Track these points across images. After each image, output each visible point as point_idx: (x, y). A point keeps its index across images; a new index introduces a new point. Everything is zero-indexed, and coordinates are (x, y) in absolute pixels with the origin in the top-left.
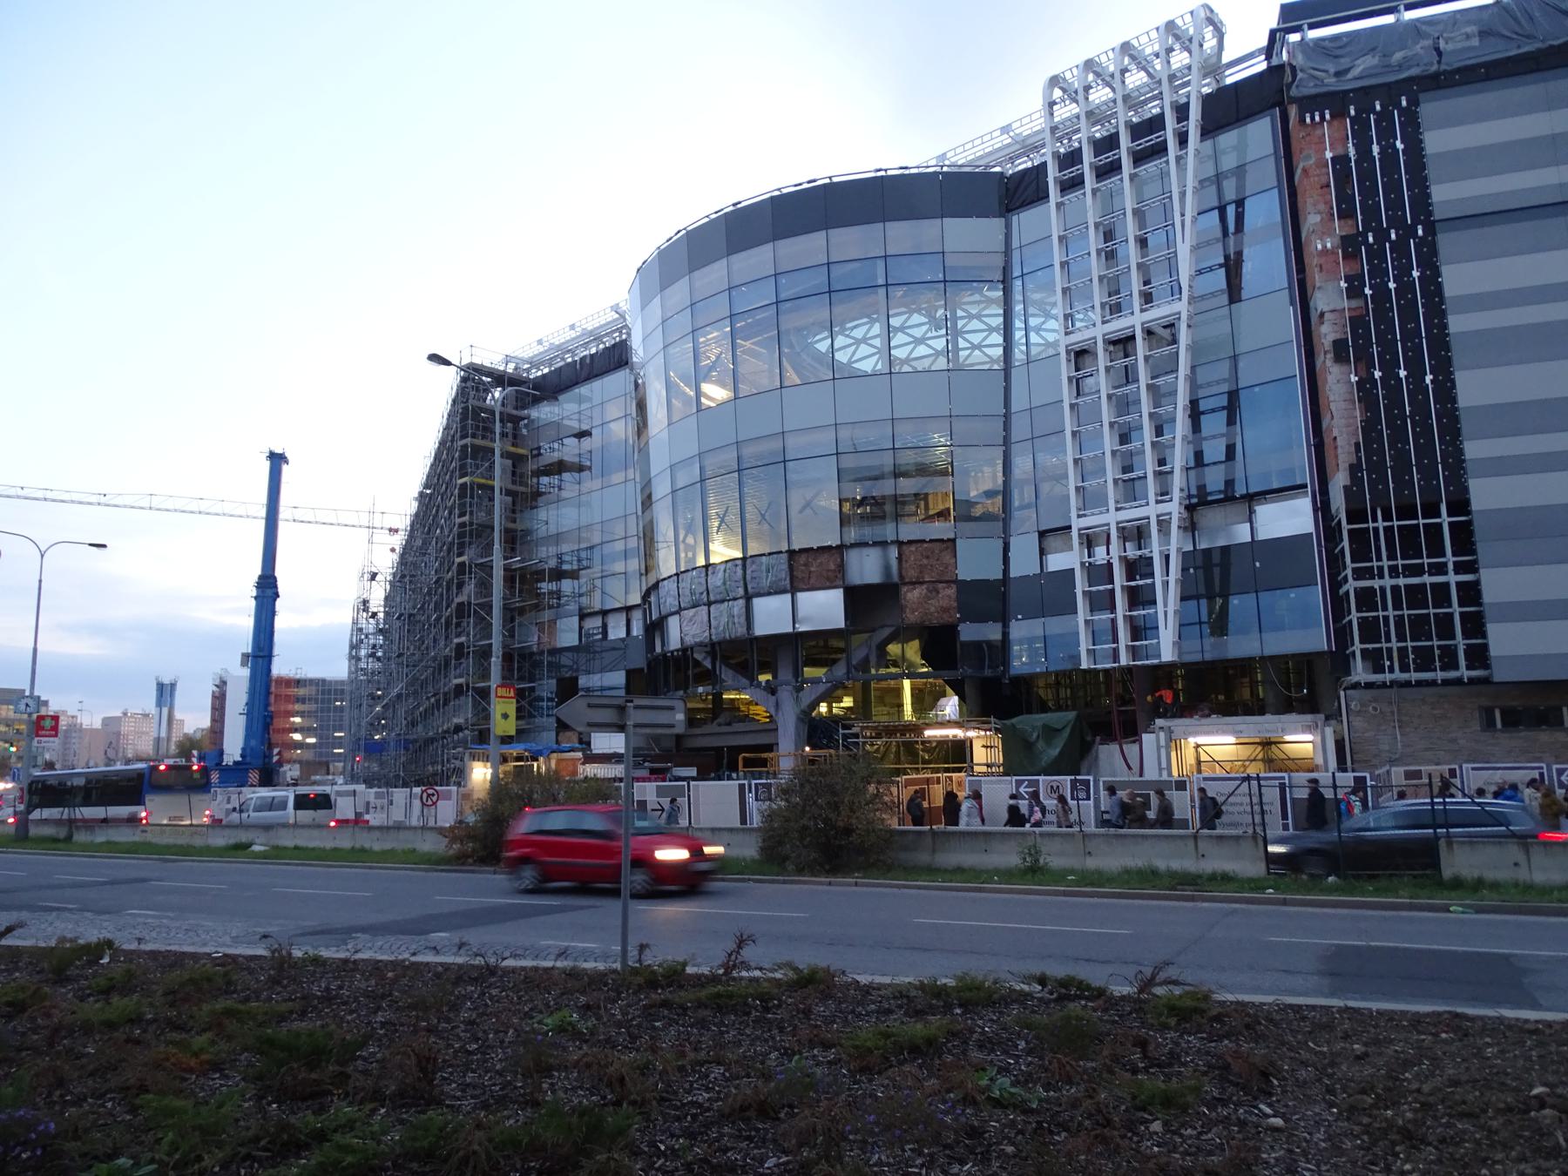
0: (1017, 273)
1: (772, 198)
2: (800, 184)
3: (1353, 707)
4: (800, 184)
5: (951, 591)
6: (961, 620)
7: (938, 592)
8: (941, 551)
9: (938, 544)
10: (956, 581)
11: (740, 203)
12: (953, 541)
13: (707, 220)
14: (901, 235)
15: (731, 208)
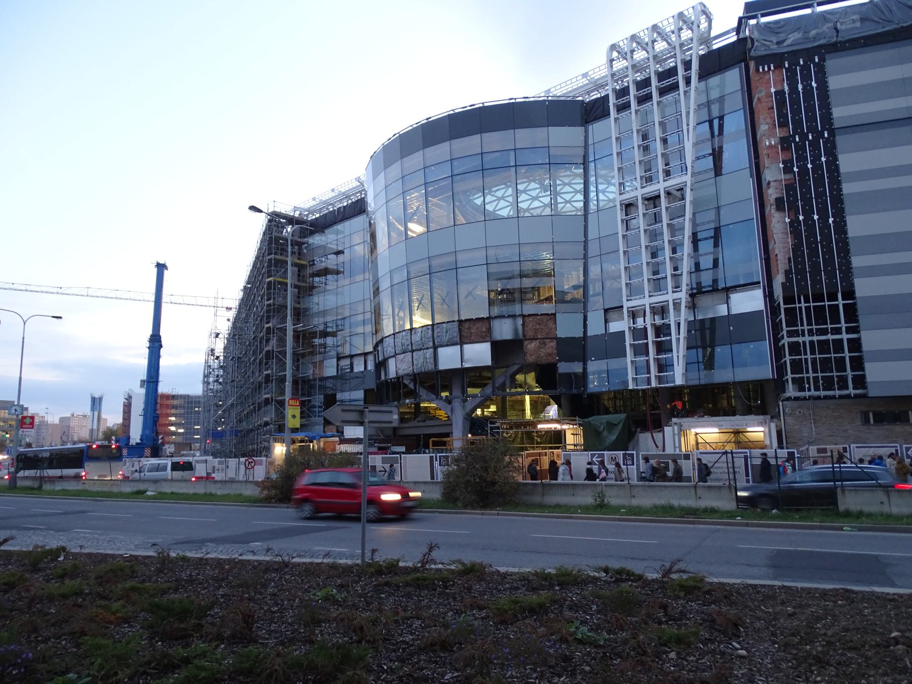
0: (591, 159)
1: (449, 115)
2: (465, 107)
3: (787, 411)
4: (465, 107)
5: (553, 344)
6: (559, 361)
7: (546, 345)
8: (547, 321)
9: (546, 316)
10: (556, 338)
11: (430, 118)
12: (554, 315)
13: (411, 128)
14: (524, 137)
15: (425, 121)
